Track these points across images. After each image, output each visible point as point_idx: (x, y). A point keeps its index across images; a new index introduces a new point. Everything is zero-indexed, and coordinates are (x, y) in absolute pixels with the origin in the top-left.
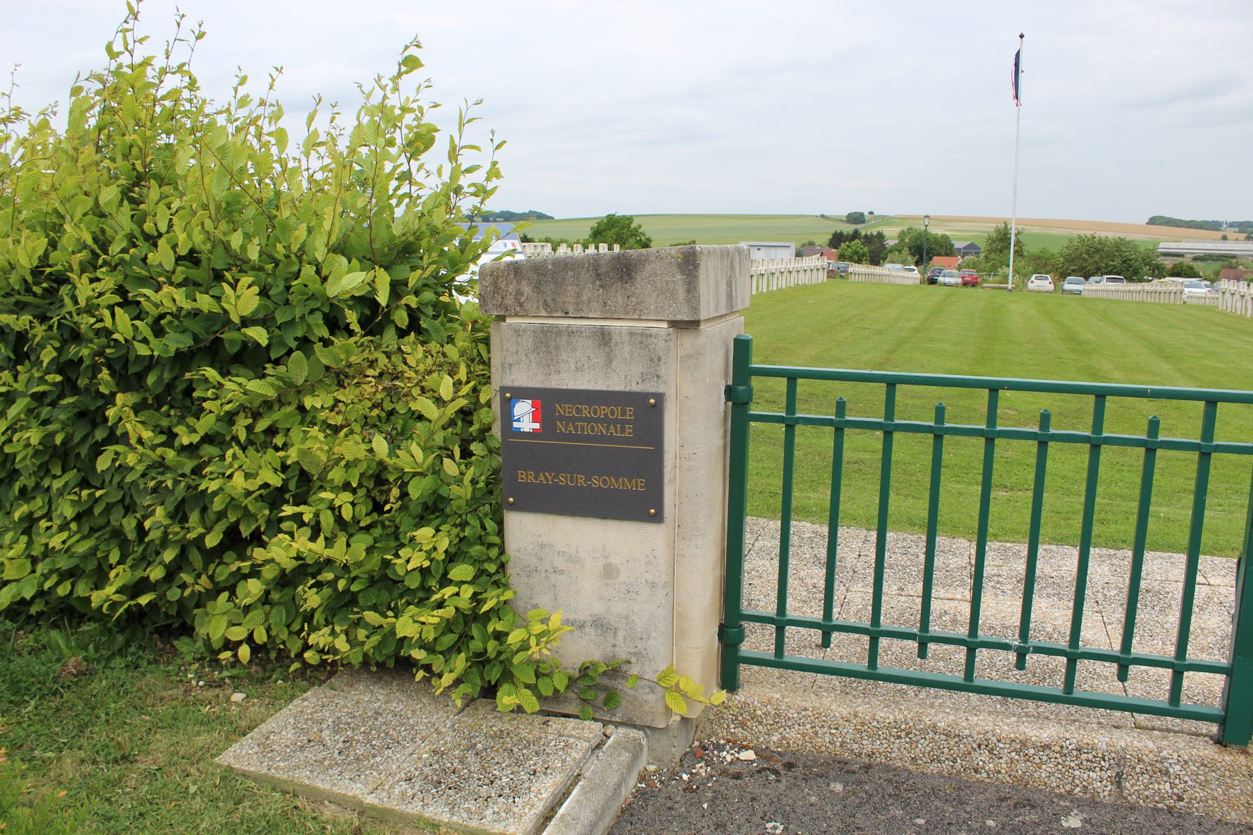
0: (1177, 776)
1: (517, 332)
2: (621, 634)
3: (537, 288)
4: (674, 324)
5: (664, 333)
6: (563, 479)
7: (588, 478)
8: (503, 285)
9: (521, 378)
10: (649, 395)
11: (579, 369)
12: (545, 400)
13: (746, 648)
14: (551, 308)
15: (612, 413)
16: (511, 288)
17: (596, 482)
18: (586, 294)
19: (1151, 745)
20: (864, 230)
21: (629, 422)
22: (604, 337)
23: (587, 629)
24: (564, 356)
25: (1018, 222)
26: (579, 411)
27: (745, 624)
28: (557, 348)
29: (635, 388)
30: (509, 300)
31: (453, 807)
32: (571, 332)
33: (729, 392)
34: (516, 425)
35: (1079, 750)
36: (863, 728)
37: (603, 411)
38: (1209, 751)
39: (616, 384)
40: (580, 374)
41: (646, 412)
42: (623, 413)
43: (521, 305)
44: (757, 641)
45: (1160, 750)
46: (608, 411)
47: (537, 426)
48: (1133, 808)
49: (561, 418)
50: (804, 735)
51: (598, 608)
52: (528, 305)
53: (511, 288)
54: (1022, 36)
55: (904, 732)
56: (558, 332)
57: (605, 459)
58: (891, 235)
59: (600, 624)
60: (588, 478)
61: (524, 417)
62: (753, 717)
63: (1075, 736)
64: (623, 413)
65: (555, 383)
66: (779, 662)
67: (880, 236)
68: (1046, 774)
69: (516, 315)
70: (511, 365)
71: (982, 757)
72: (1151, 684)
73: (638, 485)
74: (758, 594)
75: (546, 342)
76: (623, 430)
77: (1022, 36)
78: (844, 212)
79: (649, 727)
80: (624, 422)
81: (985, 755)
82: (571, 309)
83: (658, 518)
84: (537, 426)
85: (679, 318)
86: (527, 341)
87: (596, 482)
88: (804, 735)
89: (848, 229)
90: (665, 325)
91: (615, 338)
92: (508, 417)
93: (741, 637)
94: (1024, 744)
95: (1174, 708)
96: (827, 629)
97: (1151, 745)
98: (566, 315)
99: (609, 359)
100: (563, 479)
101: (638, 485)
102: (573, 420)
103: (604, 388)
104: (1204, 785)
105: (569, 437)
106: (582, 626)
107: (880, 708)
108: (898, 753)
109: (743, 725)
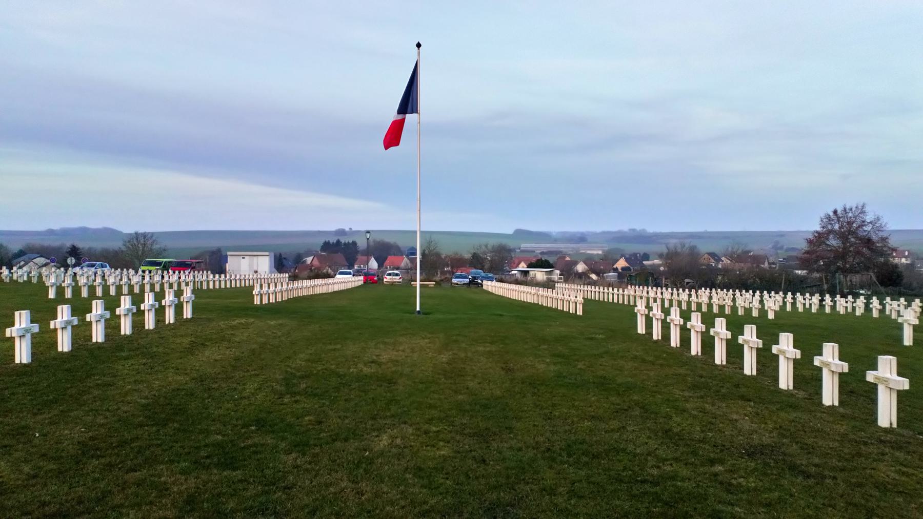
20: (343, 240)
54: (419, 45)
58: (362, 244)
67: (354, 243)
77: (419, 45)
89: (333, 240)
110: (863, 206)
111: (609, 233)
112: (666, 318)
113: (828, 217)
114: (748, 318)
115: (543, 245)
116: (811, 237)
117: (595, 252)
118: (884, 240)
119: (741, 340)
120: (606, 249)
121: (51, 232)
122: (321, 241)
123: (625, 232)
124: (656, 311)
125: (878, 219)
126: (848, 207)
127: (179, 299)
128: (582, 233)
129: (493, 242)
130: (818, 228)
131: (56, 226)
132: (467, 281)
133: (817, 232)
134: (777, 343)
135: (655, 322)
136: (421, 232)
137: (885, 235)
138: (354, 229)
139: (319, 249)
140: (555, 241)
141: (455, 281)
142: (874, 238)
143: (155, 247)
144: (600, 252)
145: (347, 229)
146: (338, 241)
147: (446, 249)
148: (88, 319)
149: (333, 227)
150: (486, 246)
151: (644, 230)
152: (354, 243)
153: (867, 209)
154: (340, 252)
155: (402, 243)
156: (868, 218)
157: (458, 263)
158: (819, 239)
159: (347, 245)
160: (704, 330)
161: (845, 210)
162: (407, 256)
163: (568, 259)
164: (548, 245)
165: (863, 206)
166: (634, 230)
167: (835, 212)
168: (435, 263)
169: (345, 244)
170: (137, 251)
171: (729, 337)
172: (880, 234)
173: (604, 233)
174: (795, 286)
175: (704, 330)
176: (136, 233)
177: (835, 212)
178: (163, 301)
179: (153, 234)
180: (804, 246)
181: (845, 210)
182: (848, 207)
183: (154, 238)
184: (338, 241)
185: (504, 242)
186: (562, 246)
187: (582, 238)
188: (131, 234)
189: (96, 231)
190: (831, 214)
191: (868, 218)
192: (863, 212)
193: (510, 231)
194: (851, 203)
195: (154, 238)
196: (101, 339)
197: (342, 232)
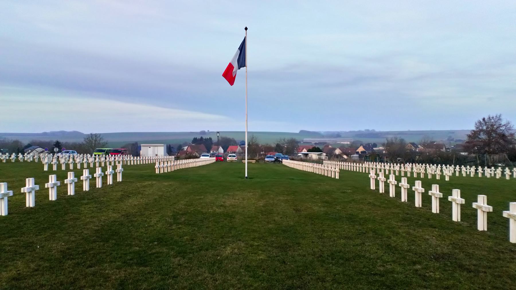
20: (204, 137)
54: (246, 29)
58: (215, 139)
67: (210, 139)
77: (246, 29)
89: (199, 137)
110: (500, 116)
111: (354, 132)
112: (411, 188)
113: (480, 122)
114: (434, 180)
117: (346, 143)
118: (512, 135)
119: (430, 193)
120: (352, 141)
121: (45, 134)
122: (192, 138)
123: (363, 132)
124: (381, 176)
125: (509, 123)
126: (491, 116)
127: (105, 173)
128: (338, 132)
129: (288, 138)
130: (474, 129)
131: (48, 131)
132: (273, 159)
134: (476, 201)
135: (380, 183)
136: (248, 133)
137: (512, 132)
138: (210, 131)
139: (191, 142)
140: (323, 136)
141: (266, 159)
142: (507, 134)
144: (349, 143)
145: (206, 131)
146: (202, 138)
147: (262, 142)
148: (65, 182)
149: (198, 130)
150: (284, 140)
151: (373, 130)
152: (210, 139)
153: (502, 117)
154: (202, 143)
155: (237, 139)
157: (268, 149)
158: (474, 135)
159: (206, 140)
160: (409, 187)
161: (489, 118)
162: (240, 146)
163: (330, 147)
165: (500, 116)
166: (368, 130)
167: (484, 119)
168: (255, 150)
169: (205, 139)
170: (92, 143)
171: (423, 191)
172: (510, 132)
173: (350, 132)
174: (461, 162)
175: (409, 187)
176: (91, 134)
177: (484, 119)
178: (95, 175)
179: (100, 134)
180: (466, 139)
181: (489, 118)
182: (491, 116)
183: (101, 137)
184: (202, 138)
185: (294, 137)
187: (338, 135)
188: (88, 135)
190: (482, 120)
192: (500, 119)
193: (298, 132)
194: (493, 114)
195: (101, 137)
196: (72, 193)
197: (203, 133)
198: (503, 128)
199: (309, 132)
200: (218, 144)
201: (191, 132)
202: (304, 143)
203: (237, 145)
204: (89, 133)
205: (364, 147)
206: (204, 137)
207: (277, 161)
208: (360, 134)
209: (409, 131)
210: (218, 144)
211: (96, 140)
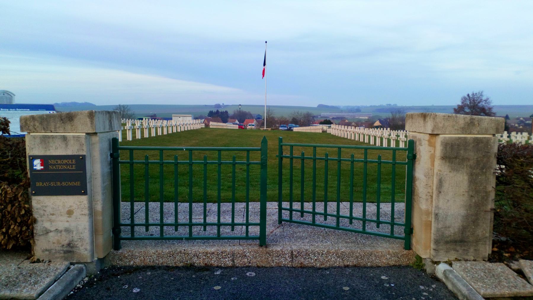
0: (249, 256)
1: (34, 137)
2: (75, 233)
3: (41, 123)
4: (87, 134)
5: (84, 137)
6: (52, 184)
7: (61, 183)
8: (28, 123)
9: (36, 152)
10: (79, 156)
11: (56, 148)
12: (44, 159)
13: (123, 235)
14: (45, 130)
15: (68, 162)
16: (32, 124)
17: (64, 184)
18: (58, 125)
19: (241, 248)
21: (73, 164)
22: (64, 138)
23: (63, 233)
24: (51, 145)
25: (268, 107)
26: (57, 162)
27: (122, 227)
28: (48, 142)
29: (75, 154)
30: (31, 128)
31: (11, 291)
32: (53, 137)
33: (111, 155)
34: (35, 168)
35: (222, 253)
36: (159, 256)
37: (65, 161)
38: (256, 248)
39: (69, 153)
40: (57, 150)
41: (80, 161)
42: (72, 162)
43: (35, 129)
44: (125, 233)
45: (244, 249)
46: (67, 161)
47: (42, 167)
48: (237, 267)
49: (51, 165)
50: (141, 260)
51: (66, 225)
52: (37, 129)
53: (32, 124)
54: (266, 42)
55: (171, 255)
56: (49, 137)
57: (68, 177)
58: (231, 112)
59: (67, 231)
60: (61, 183)
61: (38, 165)
62: (125, 257)
63: (222, 249)
64: (72, 162)
65: (48, 153)
66: (133, 238)
67: (226, 112)
68: (214, 262)
69: (34, 132)
70: (32, 149)
71: (195, 260)
72: (240, 231)
73: (78, 184)
74: (124, 219)
75: (45, 140)
76: (72, 167)
77: (266, 42)
78: (214, 104)
79: (86, 263)
80: (72, 165)
81: (196, 258)
82: (53, 130)
83: (85, 193)
84: (42, 167)
85: (89, 132)
86: (38, 141)
87: (64, 184)
88: (141, 260)
89: (214, 110)
90: (85, 134)
91: (68, 138)
92: (32, 165)
93: (120, 232)
94: (207, 253)
95: (392, 236)
96: (147, 225)
97: (241, 248)
98: (51, 132)
99: (67, 145)
100: (52, 184)
101: (78, 184)
102: (55, 165)
103: (65, 154)
104: (255, 258)
105: (54, 170)
106: (61, 231)
107: (165, 249)
108: (170, 262)
109: (121, 260)
110: (482, 92)
111: (374, 106)
115: (334, 114)
116: (456, 108)
118: (490, 109)
122: (207, 111)
124: (335, 130)
125: (488, 99)
126: (475, 93)
128: (359, 107)
129: (305, 112)
130: (460, 104)
132: (286, 128)
133: (458, 105)
136: (267, 106)
138: (225, 104)
139: (207, 115)
140: (342, 111)
141: (280, 128)
142: (486, 108)
143: (129, 113)
144: (367, 118)
145: (221, 104)
146: (218, 111)
147: (277, 115)
150: (298, 113)
151: (395, 105)
152: (226, 112)
153: (484, 94)
154: (219, 114)
155: (254, 112)
156: (484, 98)
157: (284, 122)
161: (473, 94)
162: (256, 119)
163: (347, 121)
164: (337, 114)
165: (482, 92)
166: (390, 105)
167: (468, 95)
168: (272, 122)
169: (221, 112)
173: (371, 106)
177: (468, 95)
179: (128, 106)
181: (473, 94)
182: (475, 93)
184: (218, 111)
185: (310, 111)
186: (343, 114)
188: (117, 106)
189: (98, 106)
190: (467, 96)
191: (484, 98)
192: (481, 95)
197: (218, 106)
198: (483, 103)
199: (327, 107)
200: (234, 117)
201: (206, 105)
202: (321, 117)
203: (253, 119)
204: (118, 104)
205: (380, 122)
206: (220, 111)
207: (290, 129)
208: (381, 109)
209: (433, 106)
210: (234, 117)
211: (124, 111)
